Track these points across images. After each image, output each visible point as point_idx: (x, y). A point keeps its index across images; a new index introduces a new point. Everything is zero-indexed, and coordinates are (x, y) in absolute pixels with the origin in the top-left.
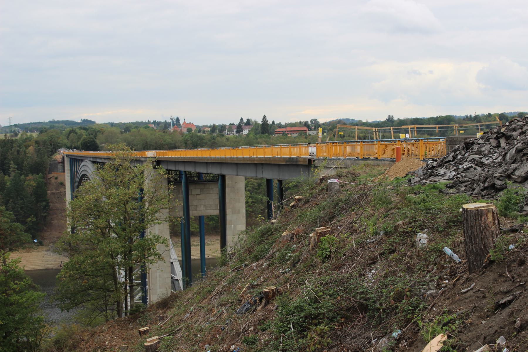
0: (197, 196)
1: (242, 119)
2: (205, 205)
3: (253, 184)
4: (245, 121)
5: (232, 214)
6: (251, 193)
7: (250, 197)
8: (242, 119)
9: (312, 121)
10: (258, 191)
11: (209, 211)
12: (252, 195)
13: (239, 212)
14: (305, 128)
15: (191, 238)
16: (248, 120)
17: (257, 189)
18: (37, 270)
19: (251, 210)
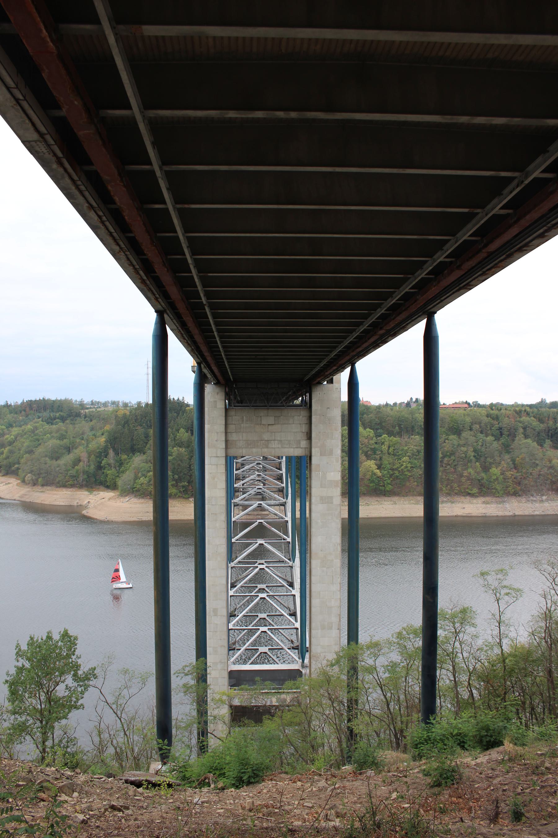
0: (270, 427)
1: (411, 399)
2: (281, 441)
3: (412, 450)
4: (414, 400)
5: (321, 455)
6: (410, 459)
7: (409, 462)
8: (411, 399)
9: (473, 403)
10: (418, 457)
11: (286, 450)
12: (411, 460)
13: (331, 453)
14: (466, 406)
15: (360, 499)
16: (417, 399)
17: (416, 455)
18: (493, 516)
19: (409, 474)
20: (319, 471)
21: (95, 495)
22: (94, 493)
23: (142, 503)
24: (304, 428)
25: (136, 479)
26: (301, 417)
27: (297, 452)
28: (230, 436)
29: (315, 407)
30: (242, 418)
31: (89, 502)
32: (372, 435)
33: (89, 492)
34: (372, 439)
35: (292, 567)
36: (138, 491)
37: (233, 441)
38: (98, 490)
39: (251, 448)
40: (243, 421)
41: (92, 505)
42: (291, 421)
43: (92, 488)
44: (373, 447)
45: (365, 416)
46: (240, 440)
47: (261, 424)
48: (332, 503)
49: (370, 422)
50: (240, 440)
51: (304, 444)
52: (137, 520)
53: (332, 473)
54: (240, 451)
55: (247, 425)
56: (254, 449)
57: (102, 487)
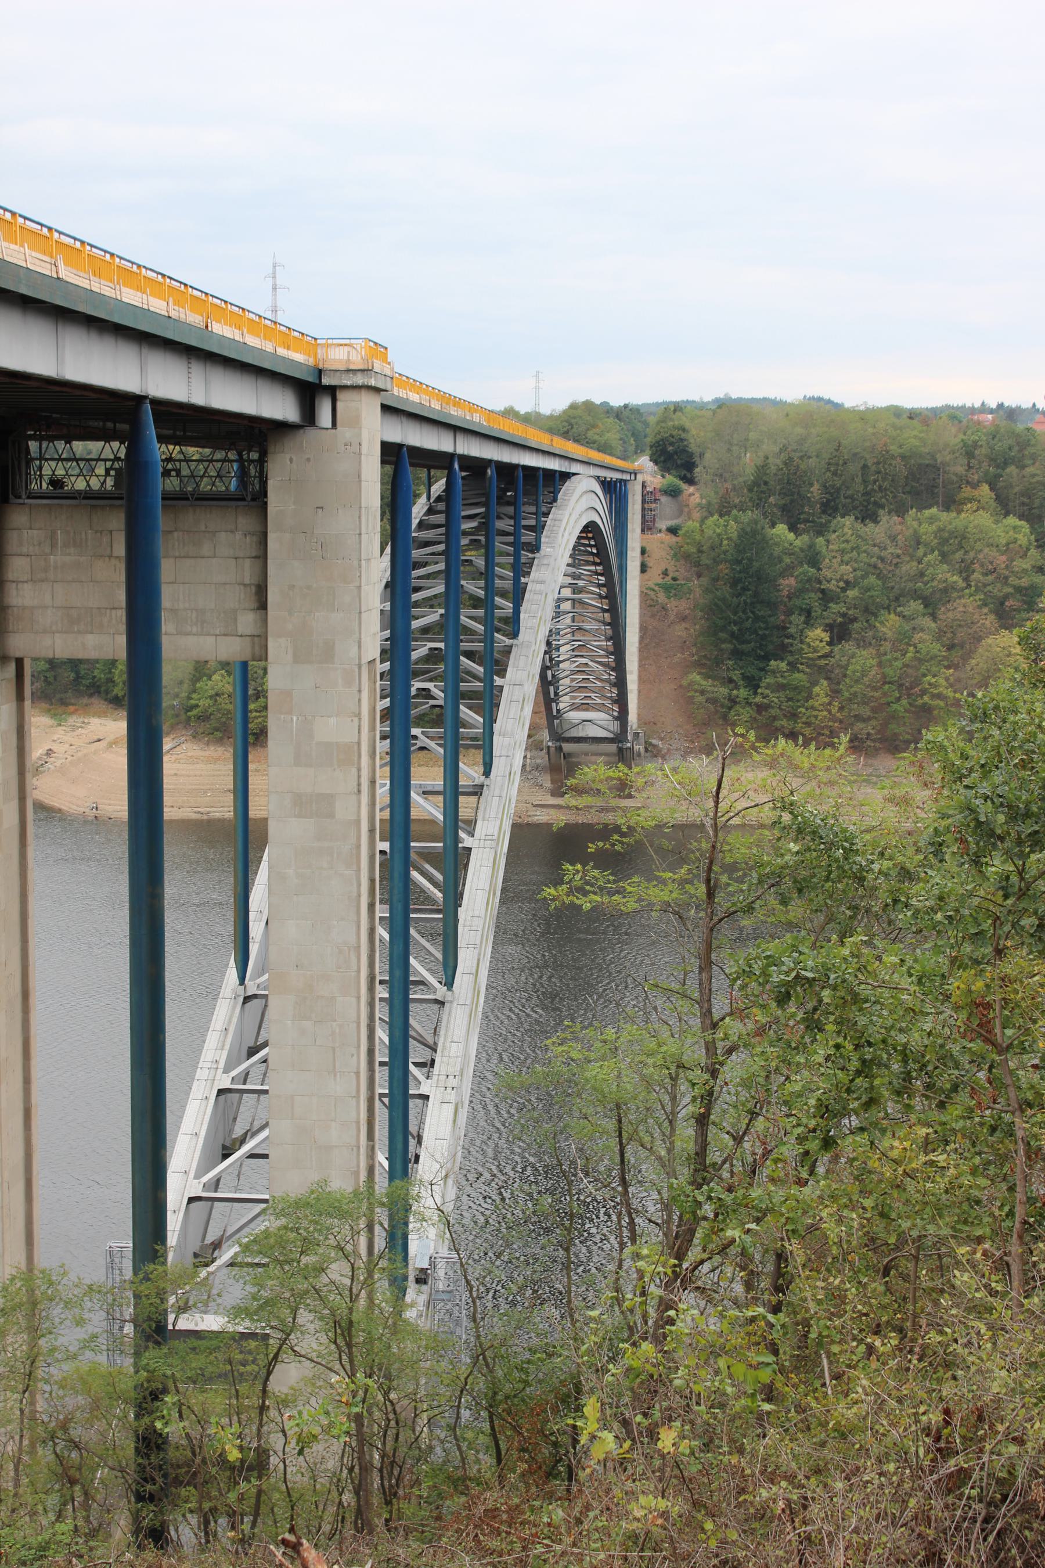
11: (191, 641)
20: (290, 712)
21: (74, 728)
22: (73, 720)
23: (216, 760)
24: (248, 572)
25: (198, 680)
26: (238, 535)
27: (232, 649)
28: (14, 592)
29: (278, 501)
30: (53, 536)
31: (49, 752)
32: (1023, 540)
33: (54, 716)
34: (1024, 555)
35: (442, 1003)
36: (204, 718)
37: (24, 608)
38: (86, 710)
39: (79, 632)
40: (53, 546)
41: (58, 763)
42: (206, 549)
43: (64, 703)
44: (1024, 582)
45: (1012, 469)
46: (46, 607)
47: (110, 556)
48: (331, 815)
49: (1027, 493)
50: (46, 607)
51: (247, 622)
52: (194, 816)
53: (332, 721)
54: (47, 641)
55: (67, 559)
56: (90, 637)
57: (98, 703)
